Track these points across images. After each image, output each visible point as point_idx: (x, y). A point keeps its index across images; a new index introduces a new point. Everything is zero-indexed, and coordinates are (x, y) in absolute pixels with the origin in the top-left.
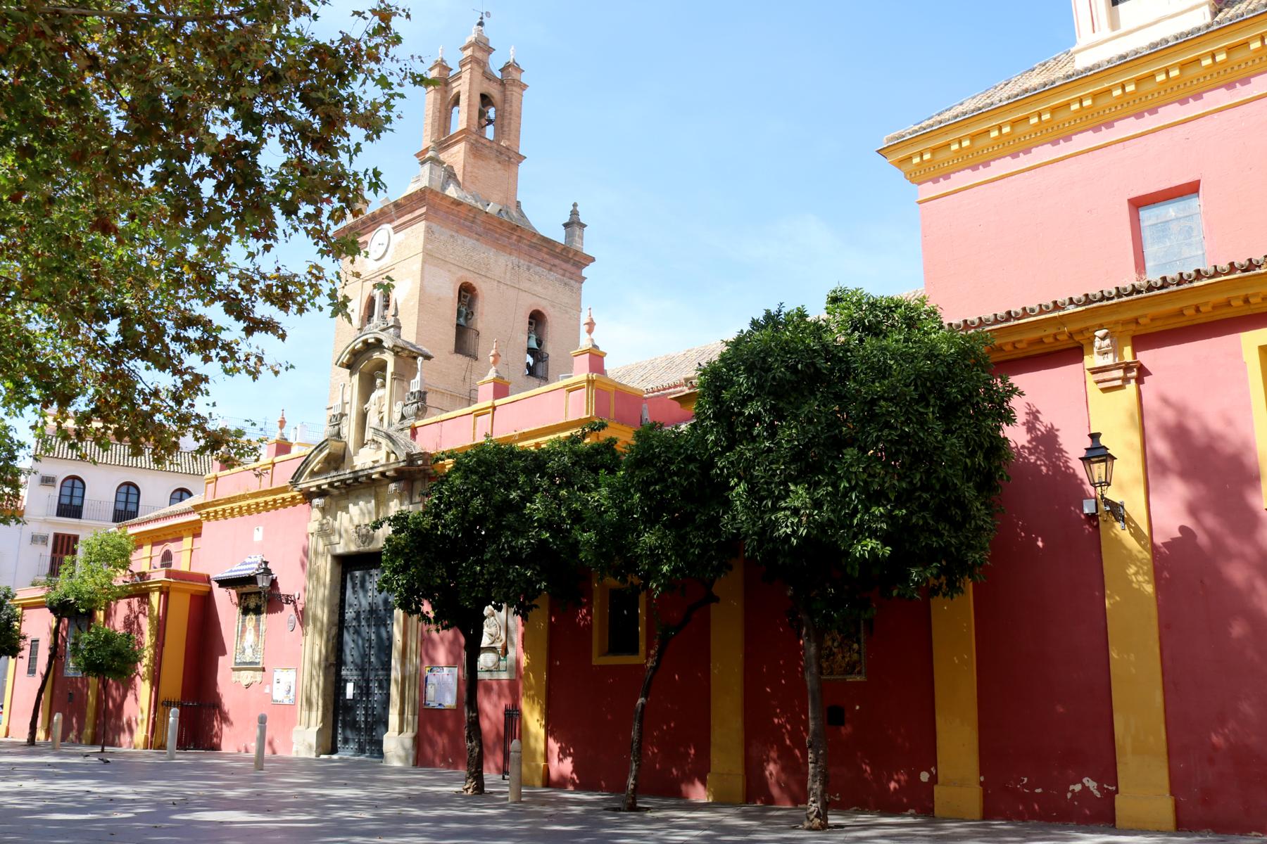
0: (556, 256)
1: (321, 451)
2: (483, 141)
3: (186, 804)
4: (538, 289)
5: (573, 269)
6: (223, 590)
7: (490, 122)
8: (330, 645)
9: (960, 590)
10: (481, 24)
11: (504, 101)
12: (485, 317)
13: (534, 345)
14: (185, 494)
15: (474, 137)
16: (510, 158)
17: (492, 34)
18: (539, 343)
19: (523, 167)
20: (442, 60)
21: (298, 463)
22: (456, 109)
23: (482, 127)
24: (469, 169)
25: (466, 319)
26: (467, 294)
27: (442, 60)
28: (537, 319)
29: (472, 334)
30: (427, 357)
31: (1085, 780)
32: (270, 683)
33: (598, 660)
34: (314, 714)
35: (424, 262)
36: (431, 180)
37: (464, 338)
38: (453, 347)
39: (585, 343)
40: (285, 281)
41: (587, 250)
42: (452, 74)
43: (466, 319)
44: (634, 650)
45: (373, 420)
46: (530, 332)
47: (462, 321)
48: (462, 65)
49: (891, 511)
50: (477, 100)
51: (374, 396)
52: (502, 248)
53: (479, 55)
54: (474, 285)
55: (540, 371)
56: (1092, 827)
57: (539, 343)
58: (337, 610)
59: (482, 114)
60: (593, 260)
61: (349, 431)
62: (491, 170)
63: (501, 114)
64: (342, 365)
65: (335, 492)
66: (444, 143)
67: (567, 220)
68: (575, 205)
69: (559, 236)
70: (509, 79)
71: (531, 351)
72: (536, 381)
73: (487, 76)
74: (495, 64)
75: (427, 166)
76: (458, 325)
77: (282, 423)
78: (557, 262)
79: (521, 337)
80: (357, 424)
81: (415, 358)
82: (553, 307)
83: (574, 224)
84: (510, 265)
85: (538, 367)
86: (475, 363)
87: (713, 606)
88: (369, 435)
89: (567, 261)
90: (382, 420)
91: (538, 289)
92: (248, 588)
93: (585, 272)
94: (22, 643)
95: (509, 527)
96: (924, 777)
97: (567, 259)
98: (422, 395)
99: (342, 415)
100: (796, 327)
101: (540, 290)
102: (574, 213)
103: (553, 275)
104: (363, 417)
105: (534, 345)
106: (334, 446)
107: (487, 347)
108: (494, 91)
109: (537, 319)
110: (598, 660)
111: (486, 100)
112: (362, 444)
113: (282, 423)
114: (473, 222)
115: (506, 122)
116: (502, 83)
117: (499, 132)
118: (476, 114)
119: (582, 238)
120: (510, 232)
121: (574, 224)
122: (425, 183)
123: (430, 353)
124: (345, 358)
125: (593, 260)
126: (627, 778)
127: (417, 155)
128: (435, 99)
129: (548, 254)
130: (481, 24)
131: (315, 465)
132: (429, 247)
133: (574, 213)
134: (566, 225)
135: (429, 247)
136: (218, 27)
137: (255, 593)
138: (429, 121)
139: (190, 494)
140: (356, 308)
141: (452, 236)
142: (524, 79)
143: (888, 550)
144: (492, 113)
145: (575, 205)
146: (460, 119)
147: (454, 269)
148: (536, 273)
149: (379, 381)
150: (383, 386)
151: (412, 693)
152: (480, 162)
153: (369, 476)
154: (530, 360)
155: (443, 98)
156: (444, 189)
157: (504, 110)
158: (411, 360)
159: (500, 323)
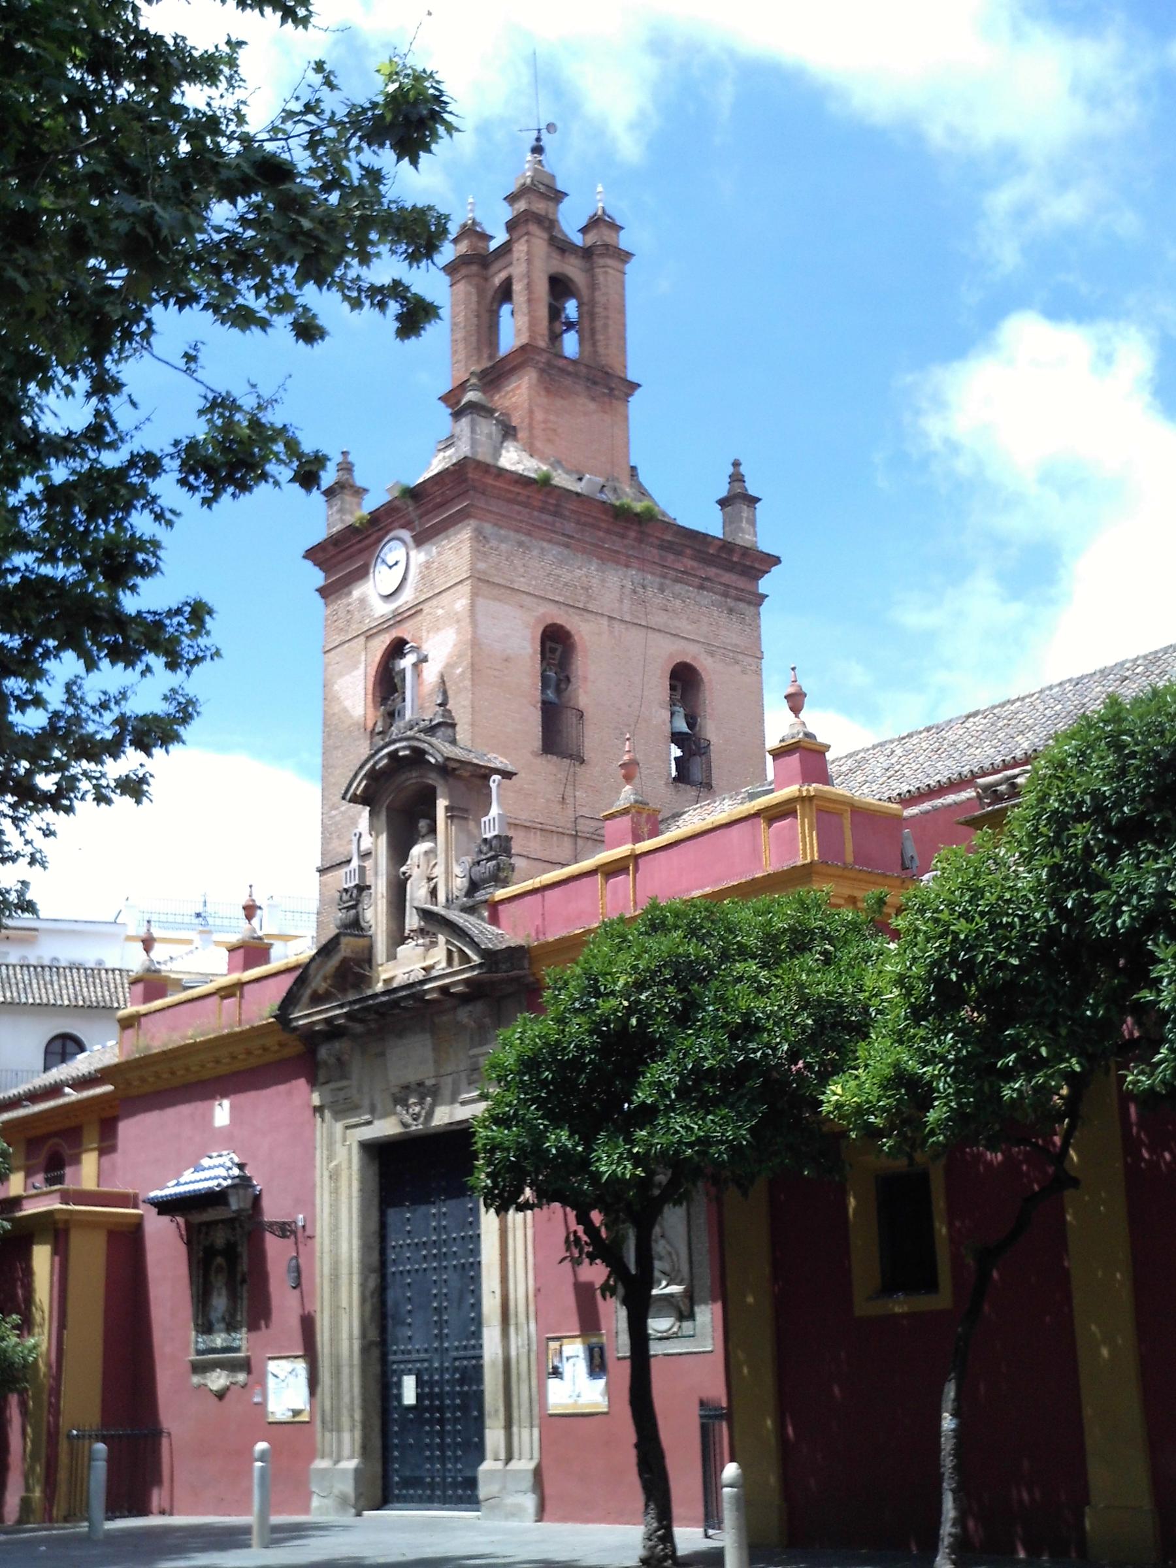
0: (709, 560)
1: (49, 1433)
2: (561, 363)
3: (376, 763)
4: (683, 625)
5: (742, 582)
6: (166, 1219)
7: (570, 325)
8: (368, 1307)
9: (632, 127)
10: (538, 150)
11: (593, 286)
12: (596, 683)
13: (682, 726)
14: (71, 1046)
15: (543, 358)
16: (609, 385)
17: (564, 168)
18: (691, 721)
19: (635, 400)
20: (474, 223)
21: (288, 981)
22: (506, 309)
23: (555, 338)
24: (539, 416)
25: (559, 691)
26: (556, 645)
27: (474, 223)
28: (684, 681)
29: (570, 717)
30: (507, 775)
31: (44, 642)
32: (262, 1384)
33: (864, 1306)
34: (346, 1437)
35: (474, 595)
36: (474, 443)
37: (557, 729)
38: (537, 744)
39: (778, 726)
40: (149, 456)
41: (766, 544)
42: (493, 245)
43: (559, 691)
44: (931, 1285)
45: (417, 893)
46: (673, 703)
47: (551, 694)
48: (511, 226)
49: (1144, 814)
50: (542, 288)
51: (418, 850)
52: (610, 557)
53: (540, 206)
54: (568, 627)
55: (697, 773)
56: (378, 689)
57: (691, 721)
58: (374, 1242)
59: (555, 312)
60: (776, 561)
61: (376, 914)
62: (580, 414)
63: (588, 310)
64: (354, 800)
65: (358, 1028)
66: (494, 376)
67: (723, 493)
68: (736, 464)
69: (710, 522)
70: (602, 247)
71: (677, 738)
72: (692, 792)
73: (561, 246)
74: (571, 219)
75: (465, 421)
76: (544, 703)
77: (250, 910)
78: (712, 571)
79: (660, 716)
80: (390, 903)
81: (486, 777)
82: (712, 654)
83: (738, 500)
84: (629, 585)
85: (693, 768)
86: (580, 770)
87: (1069, 1194)
88: (413, 921)
89: (730, 567)
90: (433, 892)
91: (683, 625)
92: (211, 1215)
93: (628, 268)
94: (8, 636)
95: (614, 1121)
96: (1129, 1160)
97: (730, 567)
98: (502, 846)
99: (362, 888)
100: (1006, 878)
101: (686, 624)
102: (737, 478)
103: (706, 597)
104: (399, 889)
105: (682, 726)
106: (348, 946)
107: (596, 737)
108: (573, 269)
109: (684, 681)
110: (864, 1306)
111: (560, 287)
112: (399, 937)
113: (250, 910)
114: (556, 514)
115: (599, 324)
116: (587, 253)
117: (588, 337)
118: (543, 312)
119: (753, 522)
120: (628, 529)
121: (738, 500)
122: (463, 449)
123: (510, 768)
124: (359, 786)
125: (776, 561)
126: (938, 1420)
127: (344, 798)
128: (468, 294)
129: (694, 558)
130: (538, 150)
131: (319, 983)
132: (481, 566)
133: (737, 478)
134: (723, 503)
135: (481, 566)
136: (1021, 909)
137: (223, 1221)
138: (385, 646)
139: (81, 1048)
140: (1145, 722)
141: (520, 544)
142: (625, 241)
143: (18, 46)
144: (571, 308)
145: (736, 464)
146: (512, 330)
147: (528, 601)
148: (676, 596)
149: (423, 824)
150: (433, 830)
151: (587, 829)
152: (559, 403)
153: (419, 997)
154: (676, 752)
155: (481, 292)
156: (497, 453)
157: (593, 303)
158: (478, 782)
159: (619, 683)
